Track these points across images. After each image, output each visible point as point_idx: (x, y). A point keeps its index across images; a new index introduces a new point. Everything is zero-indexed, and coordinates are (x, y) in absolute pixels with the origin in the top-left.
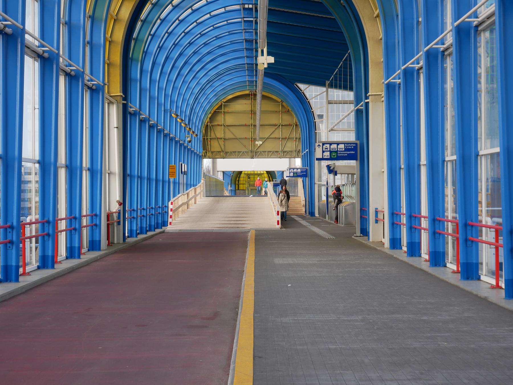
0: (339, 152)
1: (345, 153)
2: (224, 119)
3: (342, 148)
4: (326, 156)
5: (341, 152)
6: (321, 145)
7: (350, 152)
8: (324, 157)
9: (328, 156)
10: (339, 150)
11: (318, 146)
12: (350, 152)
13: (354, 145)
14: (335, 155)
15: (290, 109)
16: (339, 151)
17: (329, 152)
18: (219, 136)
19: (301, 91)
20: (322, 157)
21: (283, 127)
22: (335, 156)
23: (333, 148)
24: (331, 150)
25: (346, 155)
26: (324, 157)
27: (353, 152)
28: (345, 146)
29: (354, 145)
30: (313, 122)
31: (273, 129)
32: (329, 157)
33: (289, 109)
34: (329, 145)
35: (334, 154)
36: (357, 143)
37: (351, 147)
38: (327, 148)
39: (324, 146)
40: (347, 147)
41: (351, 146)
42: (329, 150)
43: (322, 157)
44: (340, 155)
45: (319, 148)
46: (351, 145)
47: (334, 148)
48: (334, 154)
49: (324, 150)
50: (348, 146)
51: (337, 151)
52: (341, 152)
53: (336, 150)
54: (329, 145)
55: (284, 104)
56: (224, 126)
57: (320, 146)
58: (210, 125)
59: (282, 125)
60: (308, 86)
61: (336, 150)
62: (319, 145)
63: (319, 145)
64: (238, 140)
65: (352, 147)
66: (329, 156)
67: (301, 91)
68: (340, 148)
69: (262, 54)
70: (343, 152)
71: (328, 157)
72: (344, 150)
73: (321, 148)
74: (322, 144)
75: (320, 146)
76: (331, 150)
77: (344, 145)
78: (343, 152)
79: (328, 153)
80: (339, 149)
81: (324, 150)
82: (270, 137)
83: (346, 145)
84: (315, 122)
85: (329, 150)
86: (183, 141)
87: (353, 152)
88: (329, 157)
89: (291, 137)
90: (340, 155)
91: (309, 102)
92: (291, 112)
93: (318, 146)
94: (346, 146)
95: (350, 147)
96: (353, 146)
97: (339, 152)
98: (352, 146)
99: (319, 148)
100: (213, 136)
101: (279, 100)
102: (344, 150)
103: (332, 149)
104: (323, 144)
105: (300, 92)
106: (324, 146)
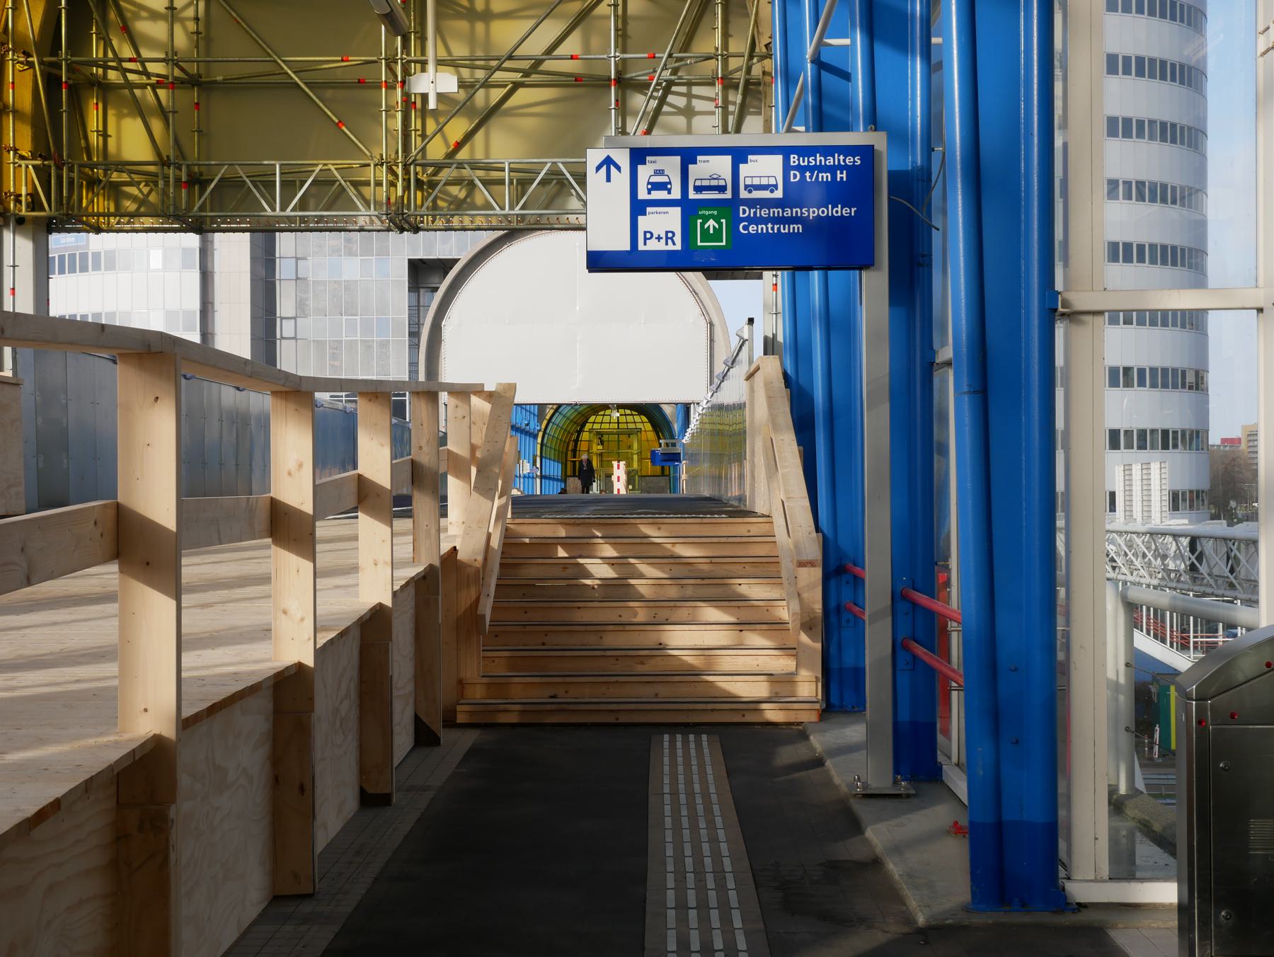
0: (744, 212)
3: (764, 182)
6: (622, 158)
9: (669, 236)
11: (598, 168)
14: (718, 232)
16: (752, 203)
22: (717, 235)
23: (706, 183)
27: (846, 212)
28: (787, 168)
34: (677, 159)
35: (711, 223)
38: (664, 179)
42: (676, 194)
45: (608, 179)
47: (714, 183)
48: (711, 223)
49: (643, 194)
51: (736, 201)
54: (677, 159)
57: (618, 168)
61: (728, 195)
62: (608, 162)
63: (608, 162)
65: (842, 176)
68: (756, 182)
73: (621, 179)
75: (618, 168)
79: (671, 220)
81: (643, 194)
83: (794, 159)
85: (676, 194)
87: (846, 212)
93: (598, 168)
99: (608, 179)
102: (779, 194)
104: (638, 156)
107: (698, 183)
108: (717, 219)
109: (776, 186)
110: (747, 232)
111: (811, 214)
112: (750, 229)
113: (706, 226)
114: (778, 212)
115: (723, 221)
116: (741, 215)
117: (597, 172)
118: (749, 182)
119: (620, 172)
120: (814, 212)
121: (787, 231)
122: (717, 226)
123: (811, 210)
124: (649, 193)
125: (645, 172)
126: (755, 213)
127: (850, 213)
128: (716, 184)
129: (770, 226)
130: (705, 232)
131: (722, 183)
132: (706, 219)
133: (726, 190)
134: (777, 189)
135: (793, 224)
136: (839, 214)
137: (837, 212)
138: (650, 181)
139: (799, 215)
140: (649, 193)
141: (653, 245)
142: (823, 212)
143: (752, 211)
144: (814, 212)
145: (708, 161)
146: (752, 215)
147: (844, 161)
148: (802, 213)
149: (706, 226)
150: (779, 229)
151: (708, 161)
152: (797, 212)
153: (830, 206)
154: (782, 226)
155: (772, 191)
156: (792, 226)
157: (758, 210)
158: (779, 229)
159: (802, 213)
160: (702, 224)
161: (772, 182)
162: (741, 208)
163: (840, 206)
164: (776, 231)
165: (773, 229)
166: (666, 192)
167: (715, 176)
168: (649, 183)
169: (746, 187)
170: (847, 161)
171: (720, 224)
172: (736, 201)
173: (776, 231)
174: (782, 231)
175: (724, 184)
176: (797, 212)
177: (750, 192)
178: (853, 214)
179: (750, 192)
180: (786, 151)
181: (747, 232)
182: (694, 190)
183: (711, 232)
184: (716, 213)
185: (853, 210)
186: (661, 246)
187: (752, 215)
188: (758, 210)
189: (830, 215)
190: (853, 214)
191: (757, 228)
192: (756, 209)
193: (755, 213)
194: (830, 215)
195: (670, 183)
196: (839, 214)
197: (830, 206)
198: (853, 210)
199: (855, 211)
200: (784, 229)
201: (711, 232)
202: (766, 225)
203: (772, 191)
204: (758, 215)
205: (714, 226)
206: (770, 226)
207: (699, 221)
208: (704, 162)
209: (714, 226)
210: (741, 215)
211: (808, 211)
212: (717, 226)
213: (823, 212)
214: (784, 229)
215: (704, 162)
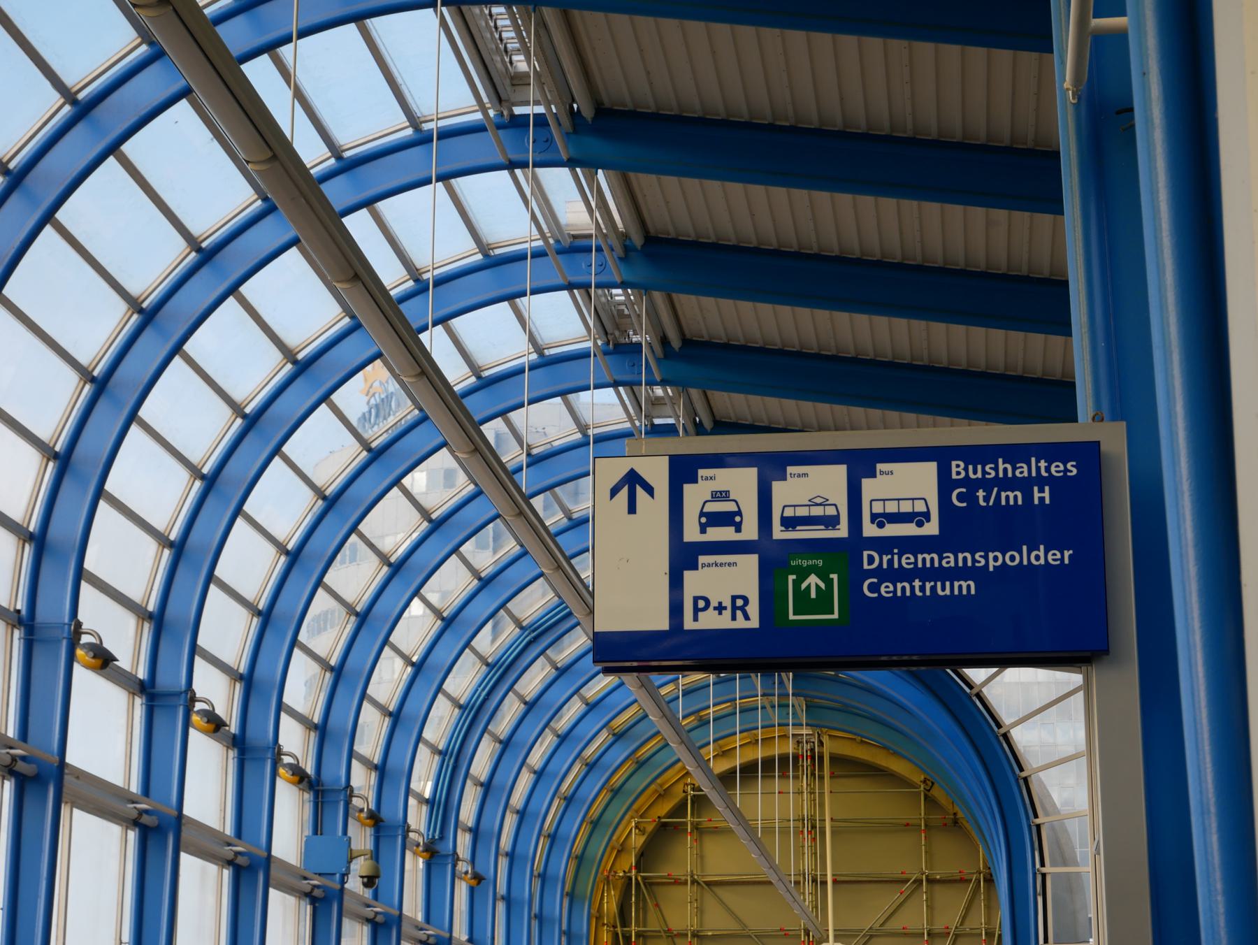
0: (871, 560)
1: (949, 561)
2: (701, 857)
3: (906, 507)
4: (720, 608)
5: (907, 561)
6: (656, 471)
7: (1012, 559)
8: (689, 624)
9: (738, 604)
10: (870, 530)
11: (614, 492)
12: (1012, 559)
13: (1056, 469)
15: (960, 815)
16: (884, 545)
17: (749, 564)
18: (676, 924)
19: (968, 690)
20: (664, 624)
21: (937, 888)
23: (803, 512)
24: (778, 533)
25: (967, 586)
26: (689, 624)
27: (1053, 557)
28: (945, 484)
29: (1056, 469)
30: (1030, 827)
31: (892, 897)
32: (754, 623)
33: (955, 814)
34: (753, 472)
35: (813, 580)
36: (1096, 444)
37: (1028, 496)
38: (728, 507)
39: (688, 489)
40: (969, 497)
41: (1024, 485)
43: (664, 624)
44: (886, 589)
45: (632, 509)
46: (1023, 471)
47: (817, 511)
48: (813, 580)
49: (692, 533)
50: (986, 484)
52: (907, 561)
53: (842, 531)
54: (753, 472)
55: (936, 792)
56: (694, 882)
57: (650, 490)
58: (636, 879)
59: (928, 880)
60: (995, 670)
61: (842, 531)
62: (633, 480)
63: (633, 480)
64: (753, 939)
66: (754, 609)
67: (968, 690)
68: (892, 508)
69: (650, 345)
70: (927, 559)
71: (740, 623)
72: (932, 528)
73: (655, 508)
74: (664, 462)
75: (650, 490)
76: (778, 533)
77: (931, 468)
78: (927, 559)
80: (880, 519)
81: (692, 533)
82: (888, 926)
83: (957, 469)
84: (1038, 827)
85: (750, 531)
86: (338, 875)
87: (1053, 557)
88: (754, 623)
89: (968, 926)
90: (886, 589)
91: (1026, 780)
92: (964, 823)
93: (614, 492)
94: (966, 482)
95: (1013, 497)
96: (1051, 480)
97: (871, 560)
98: (1041, 482)
99: (632, 509)
100: (653, 925)
101: (917, 778)
102: (932, 528)
103: (789, 523)
105: (993, 730)
106: (688, 489)
107: (789, 513)
108: (824, 576)
109: (927, 516)
110: (876, 595)
111: (991, 563)
112: (883, 590)
113: (804, 586)
114: (932, 560)
115: (834, 577)
116: (866, 566)
117: (611, 499)
118: (878, 508)
119: (611, 499)
120: (996, 559)
121: (948, 592)
122: (822, 585)
123: (991, 555)
124: (703, 531)
125: (695, 496)
126: (891, 562)
127: (1062, 559)
128: (821, 513)
129: (917, 583)
130: (802, 596)
131: (831, 511)
132: (803, 574)
133: (838, 523)
134: (928, 520)
135: (958, 581)
136: (1042, 561)
137: (1037, 558)
138: (704, 511)
139: (970, 564)
140: (703, 531)
141: (710, 621)
142: (1012, 558)
143: (885, 558)
144: (996, 559)
145: (806, 475)
146: (885, 566)
147: (1048, 469)
148: (974, 561)
149: (804, 586)
150: (933, 589)
151: (806, 475)
152: (965, 559)
153: (1025, 548)
154: (939, 584)
155: (920, 524)
156: (956, 584)
157: (896, 557)
158: (933, 589)
159: (974, 561)
160: (797, 584)
161: (920, 507)
162: (865, 553)
163: (1042, 547)
164: (928, 593)
165: (922, 589)
166: (732, 529)
167: (819, 501)
168: (702, 514)
169: (874, 517)
170: (1053, 469)
171: (829, 583)
172: (856, 541)
173: (928, 593)
174: (918, 593)
175: (924, 509)
176: (965, 559)
177: (881, 525)
178: (1066, 561)
179: (881, 525)
180: (941, 456)
181: (876, 595)
182: (782, 525)
183: (813, 595)
184: (820, 563)
185: (1067, 554)
186: (723, 622)
187: (885, 566)
188: (896, 557)
189: (1025, 562)
190: (1066, 561)
191: (1062, 555)
192: (893, 554)
193: (891, 562)
194: (1025, 562)
195: (739, 513)
196: (1042, 561)
197: (1025, 548)
198: (1067, 554)
199: (1070, 556)
200: (943, 589)
201: (813, 595)
202: (911, 582)
203: (920, 524)
204: (896, 566)
205: (817, 585)
206: (917, 583)
207: (791, 578)
208: (799, 476)
209: (817, 585)
210: (866, 566)
211: (986, 558)
212: (822, 585)
213: (1012, 558)
214: (943, 589)
215: (799, 476)
